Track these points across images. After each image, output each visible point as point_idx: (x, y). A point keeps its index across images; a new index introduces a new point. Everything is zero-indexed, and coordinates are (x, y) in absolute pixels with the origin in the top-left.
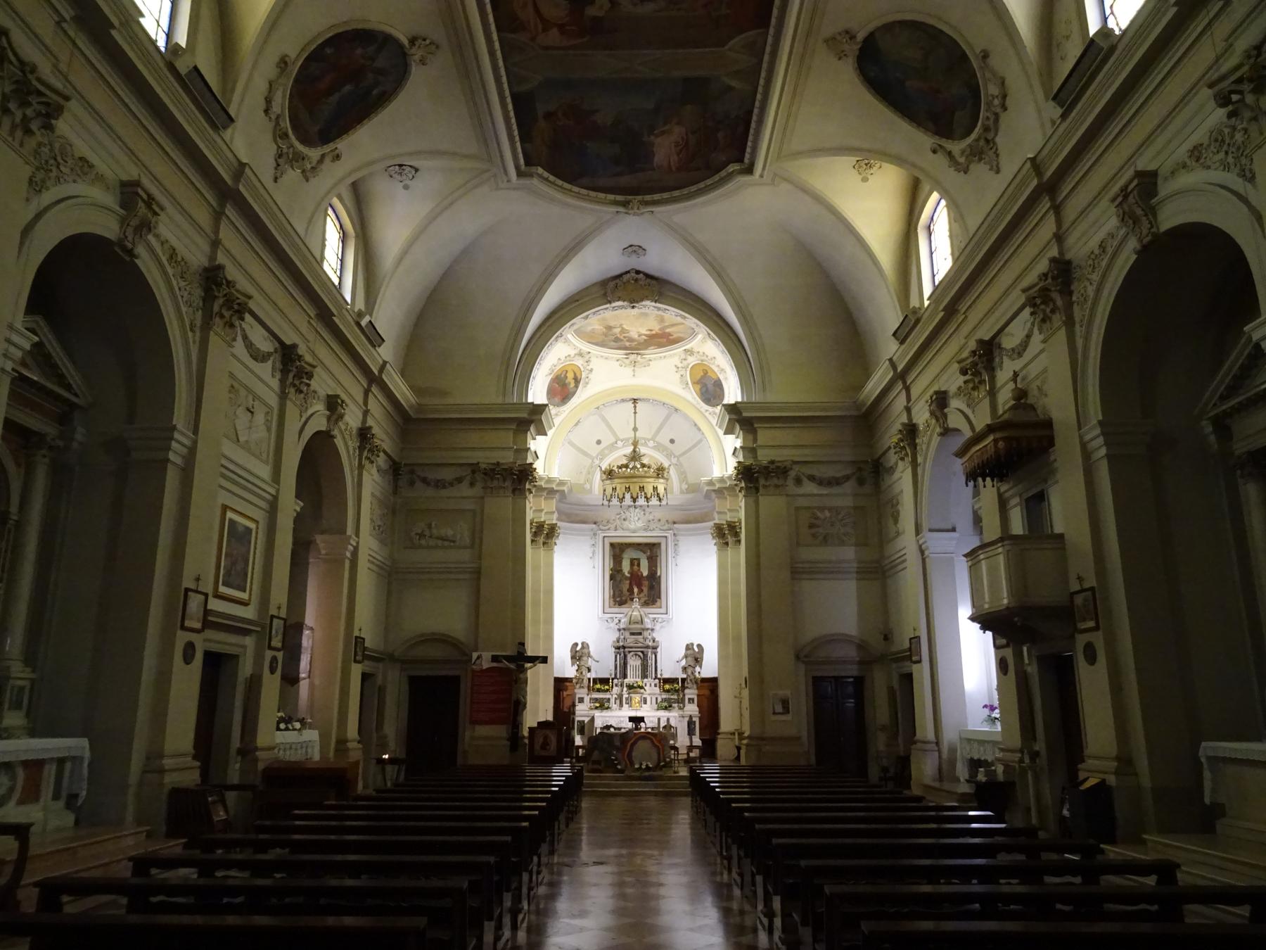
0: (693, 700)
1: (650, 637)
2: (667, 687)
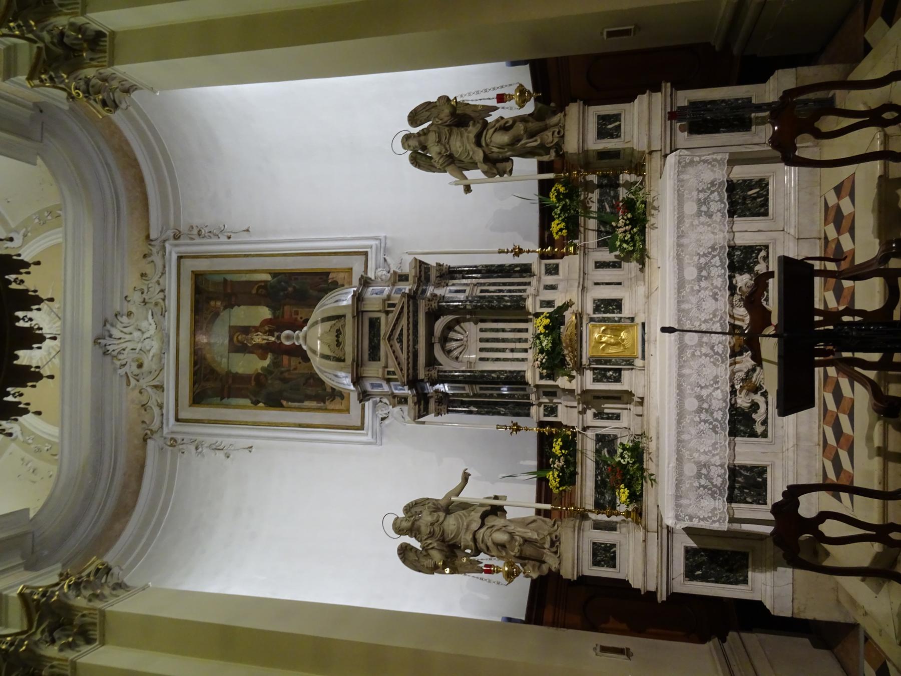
0: (604, 120)
1: (387, 290)
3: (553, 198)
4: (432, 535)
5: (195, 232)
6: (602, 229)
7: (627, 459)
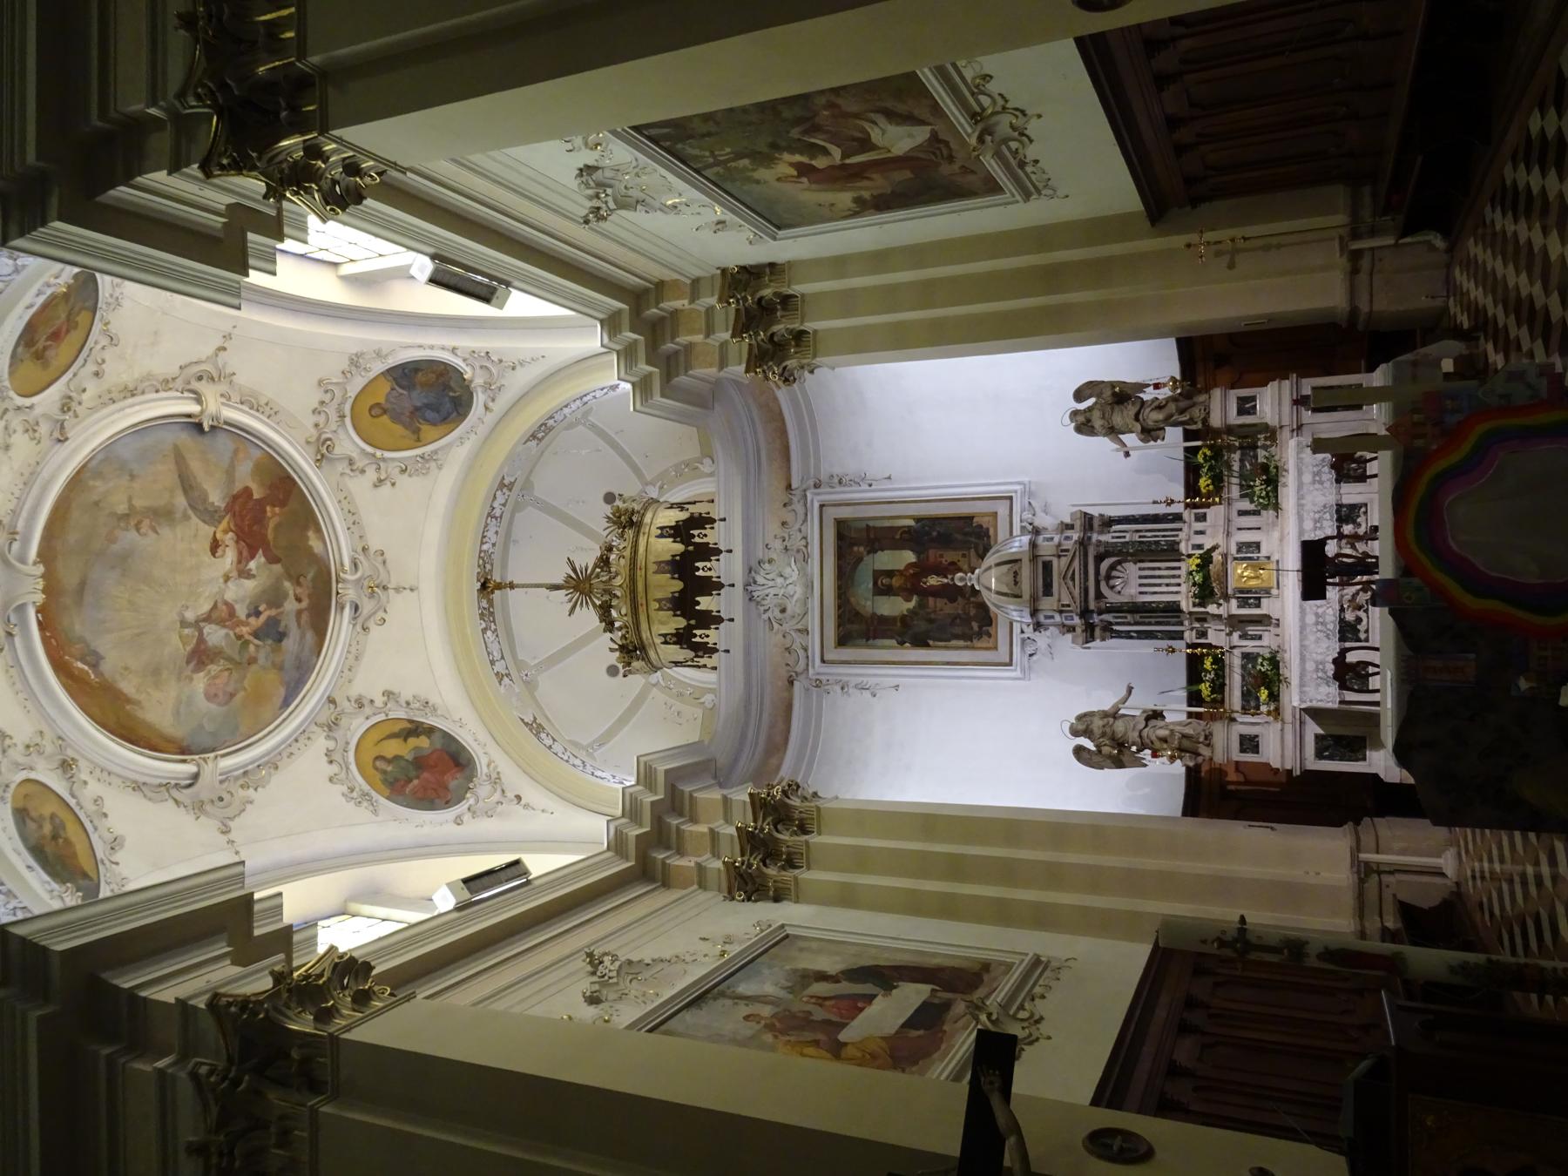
1: (1056, 539)
2: (1204, 483)
3: (1200, 458)
4: (1103, 735)
5: (836, 480)
6: (1244, 483)
7: (1266, 667)
